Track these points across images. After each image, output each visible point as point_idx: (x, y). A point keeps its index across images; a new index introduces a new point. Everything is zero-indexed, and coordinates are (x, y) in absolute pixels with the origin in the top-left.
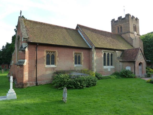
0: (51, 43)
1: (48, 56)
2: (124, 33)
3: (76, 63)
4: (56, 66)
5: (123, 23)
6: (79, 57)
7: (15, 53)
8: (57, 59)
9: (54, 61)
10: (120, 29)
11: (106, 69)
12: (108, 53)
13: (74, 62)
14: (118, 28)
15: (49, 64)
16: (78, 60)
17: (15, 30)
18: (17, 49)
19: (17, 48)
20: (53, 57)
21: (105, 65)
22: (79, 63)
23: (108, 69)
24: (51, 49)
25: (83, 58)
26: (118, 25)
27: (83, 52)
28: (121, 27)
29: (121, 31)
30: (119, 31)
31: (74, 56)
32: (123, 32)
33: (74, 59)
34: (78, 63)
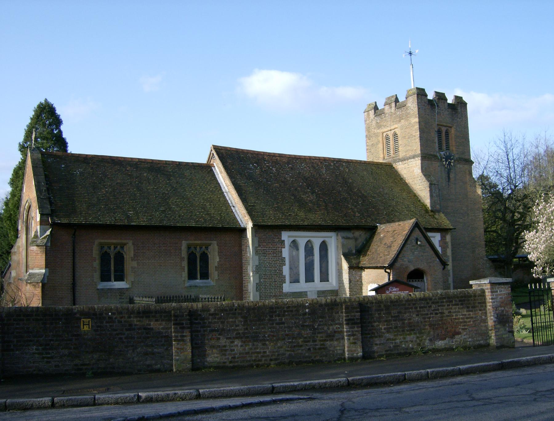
0: (108, 220)
1: (105, 258)
2: (403, 160)
3: (192, 276)
4: (128, 286)
5: (400, 121)
6: (205, 258)
7: (19, 247)
8: (129, 264)
9: (122, 271)
10: (392, 142)
11: (305, 292)
12: (309, 241)
13: (185, 274)
14: (387, 138)
15: (110, 280)
16: (198, 267)
17: (20, 144)
18: (24, 237)
19: (24, 233)
20: (120, 259)
21: (105, 278)
22: (205, 275)
23: (307, 292)
24: (113, 240)
25: (214, 259)
26: (385, 126)
27: (215, 242)
28: (395, 135)
29: (396, 150)
30: (388, 152)
31: (184, 254)
32: (401, 154)
33: (185, 264)
34: (113, 278)
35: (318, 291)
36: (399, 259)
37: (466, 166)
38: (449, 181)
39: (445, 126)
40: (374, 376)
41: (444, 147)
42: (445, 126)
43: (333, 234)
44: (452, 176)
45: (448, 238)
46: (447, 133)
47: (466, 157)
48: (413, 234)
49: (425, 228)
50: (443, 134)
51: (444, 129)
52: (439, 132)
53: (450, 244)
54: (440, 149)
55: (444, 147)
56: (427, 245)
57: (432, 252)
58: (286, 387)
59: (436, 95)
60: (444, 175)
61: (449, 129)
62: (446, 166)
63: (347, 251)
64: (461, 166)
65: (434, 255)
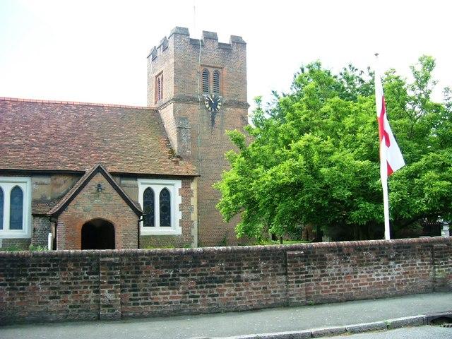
35: (4, 239)
36: (69, 207)
37: (240, 110)
38: (213, 126)
39: (213, 67)
40: (399, 319)
41: (211, 88)
42: (213, 67)
43: (27, 179)
44: (217, 120)
45: (193, 186)
46: (217, 75)
47: (241, 100)
48: (93, 179)
49: (114, 174)
50: (211, 75)
51: (211, 71)
52: (206, 73)
53: (195, 193)
54: (205, 89)
55: (211, 88)
56: (115, 193)
57: (122, 201)
58: (376, 325)
59: (204, 35)
60: (207, 119)
61: (220, 70)
62: (210, 109)
63: (38, 197)
64: (232, 109)
65: (125, 204)
